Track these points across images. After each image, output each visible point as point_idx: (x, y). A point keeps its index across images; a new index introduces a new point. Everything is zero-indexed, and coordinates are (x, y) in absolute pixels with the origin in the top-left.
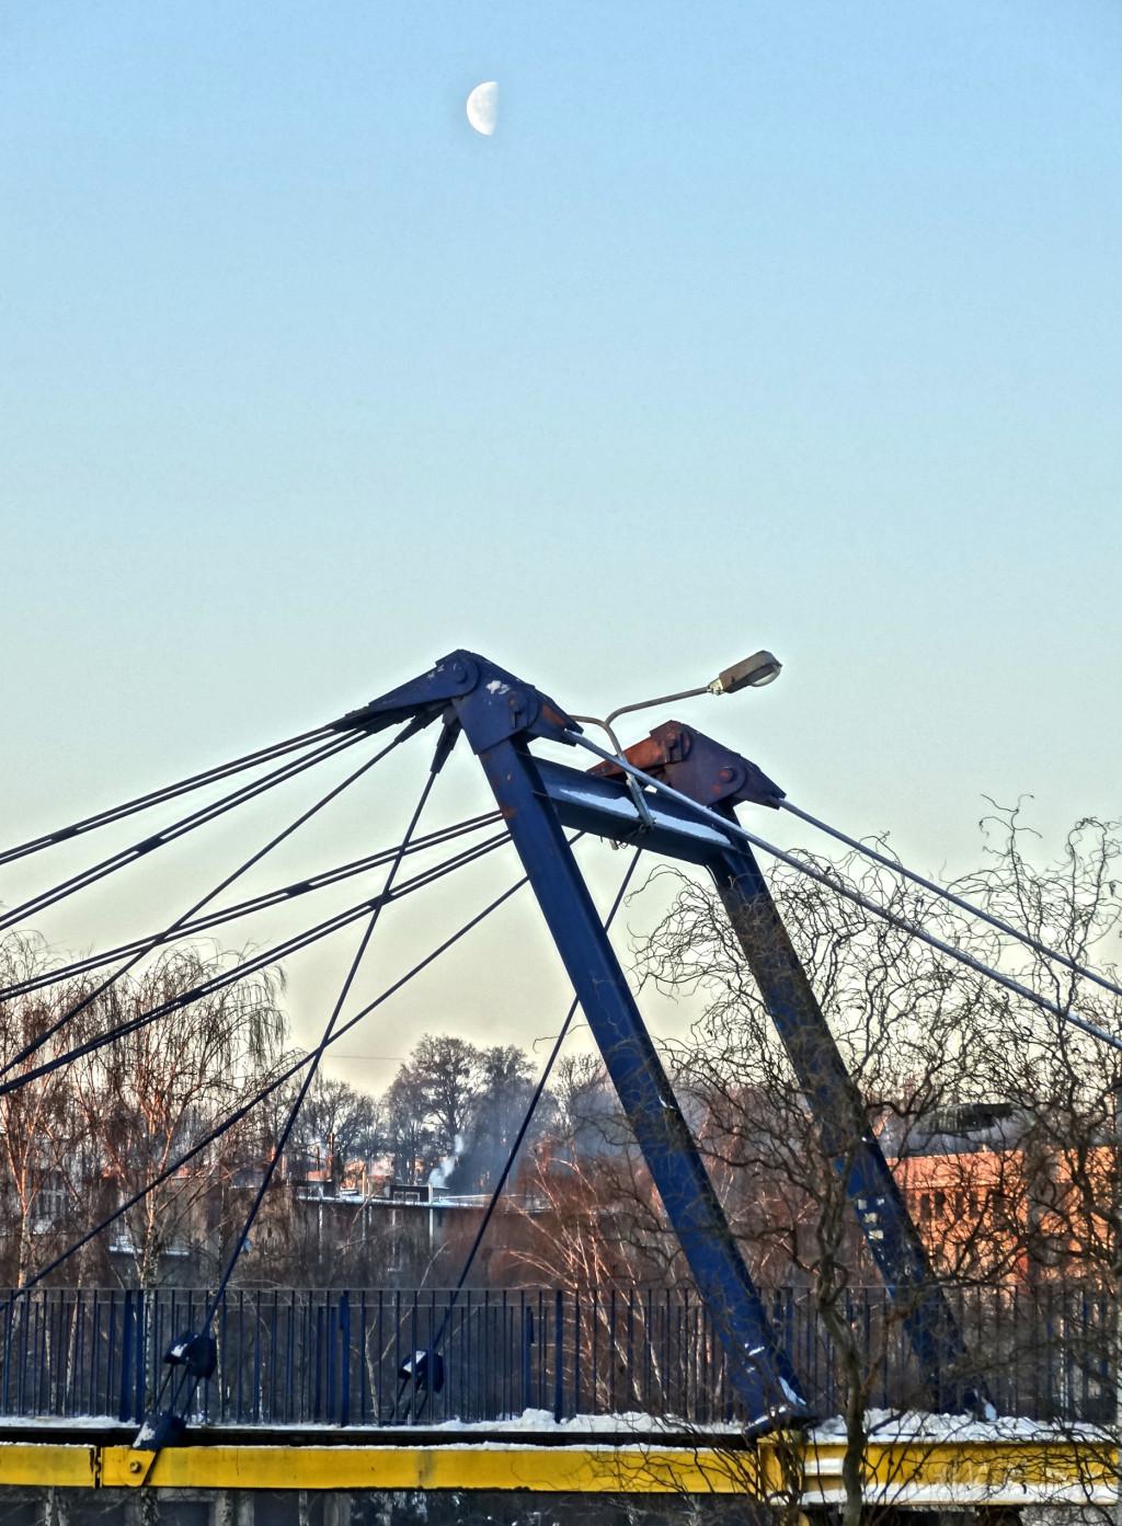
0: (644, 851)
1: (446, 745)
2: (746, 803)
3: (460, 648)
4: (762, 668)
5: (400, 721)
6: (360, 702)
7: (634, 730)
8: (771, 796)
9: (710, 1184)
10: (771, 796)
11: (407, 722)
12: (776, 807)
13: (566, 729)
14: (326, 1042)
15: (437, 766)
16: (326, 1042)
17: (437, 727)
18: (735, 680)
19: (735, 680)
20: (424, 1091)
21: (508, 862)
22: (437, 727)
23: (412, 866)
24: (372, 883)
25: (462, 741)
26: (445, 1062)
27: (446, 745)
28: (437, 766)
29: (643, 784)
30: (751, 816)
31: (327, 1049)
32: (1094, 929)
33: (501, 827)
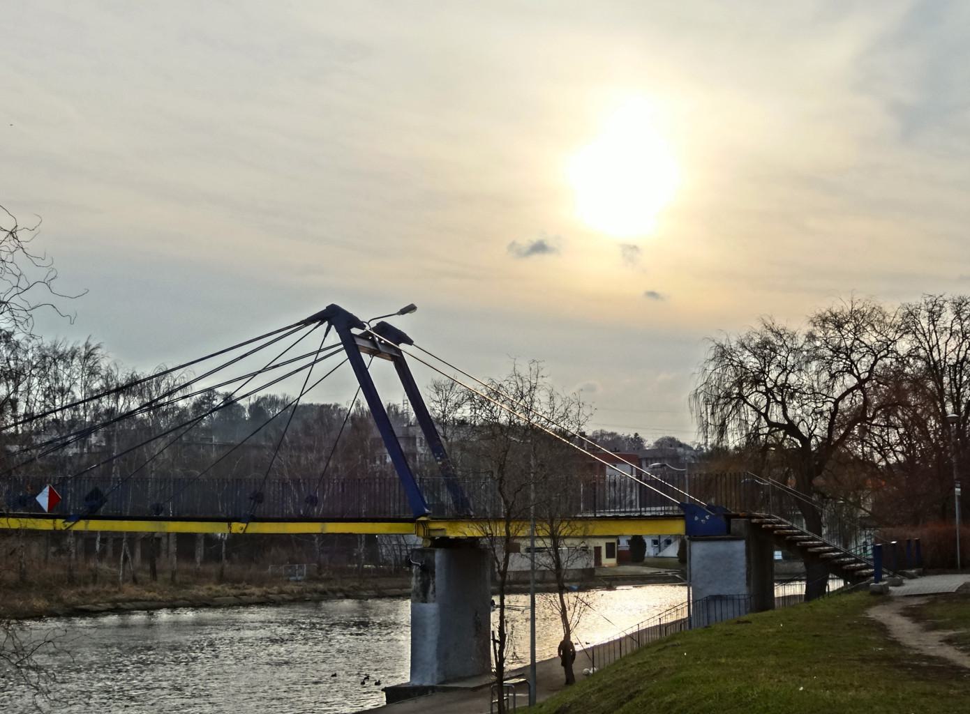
0: (344, 350)
1: (328, 329)
2: (354, 328)
3: (672, 435)
4: (411, 309)
5: (315, 323)
6: (305, 317)
7: (373, 324)
8: (410, 342)
9: (115, 533)
10: (410, 342)
11: (317, 323)
12: (411, 345)
13: (360, 325)
14: (301, 395)
15: (326, 336)
16: (301, 395)
17: (326, 324)
18: (403, 312)
19: (403, 312)
20: (203, 406)
21: (343, 355)
22: (326, 324)
23: (321, 355)
24: (312, 359)
25: (333, 326)
26: (209, 397)
27: (328, 329)
28: (326, 336)
29: (380, 340)
30: (402, 346)
31: (301, 398)
32: (536, 391)
33: (342, 346)
